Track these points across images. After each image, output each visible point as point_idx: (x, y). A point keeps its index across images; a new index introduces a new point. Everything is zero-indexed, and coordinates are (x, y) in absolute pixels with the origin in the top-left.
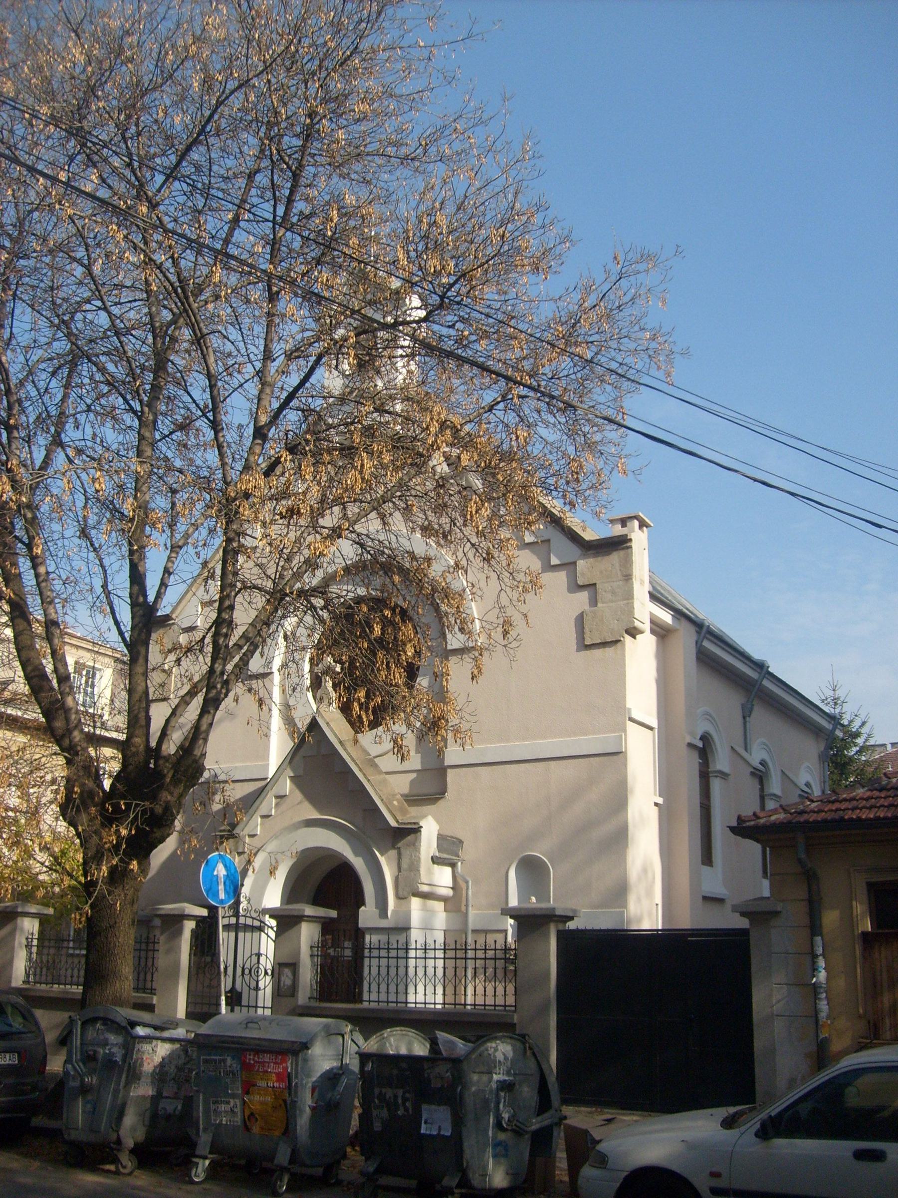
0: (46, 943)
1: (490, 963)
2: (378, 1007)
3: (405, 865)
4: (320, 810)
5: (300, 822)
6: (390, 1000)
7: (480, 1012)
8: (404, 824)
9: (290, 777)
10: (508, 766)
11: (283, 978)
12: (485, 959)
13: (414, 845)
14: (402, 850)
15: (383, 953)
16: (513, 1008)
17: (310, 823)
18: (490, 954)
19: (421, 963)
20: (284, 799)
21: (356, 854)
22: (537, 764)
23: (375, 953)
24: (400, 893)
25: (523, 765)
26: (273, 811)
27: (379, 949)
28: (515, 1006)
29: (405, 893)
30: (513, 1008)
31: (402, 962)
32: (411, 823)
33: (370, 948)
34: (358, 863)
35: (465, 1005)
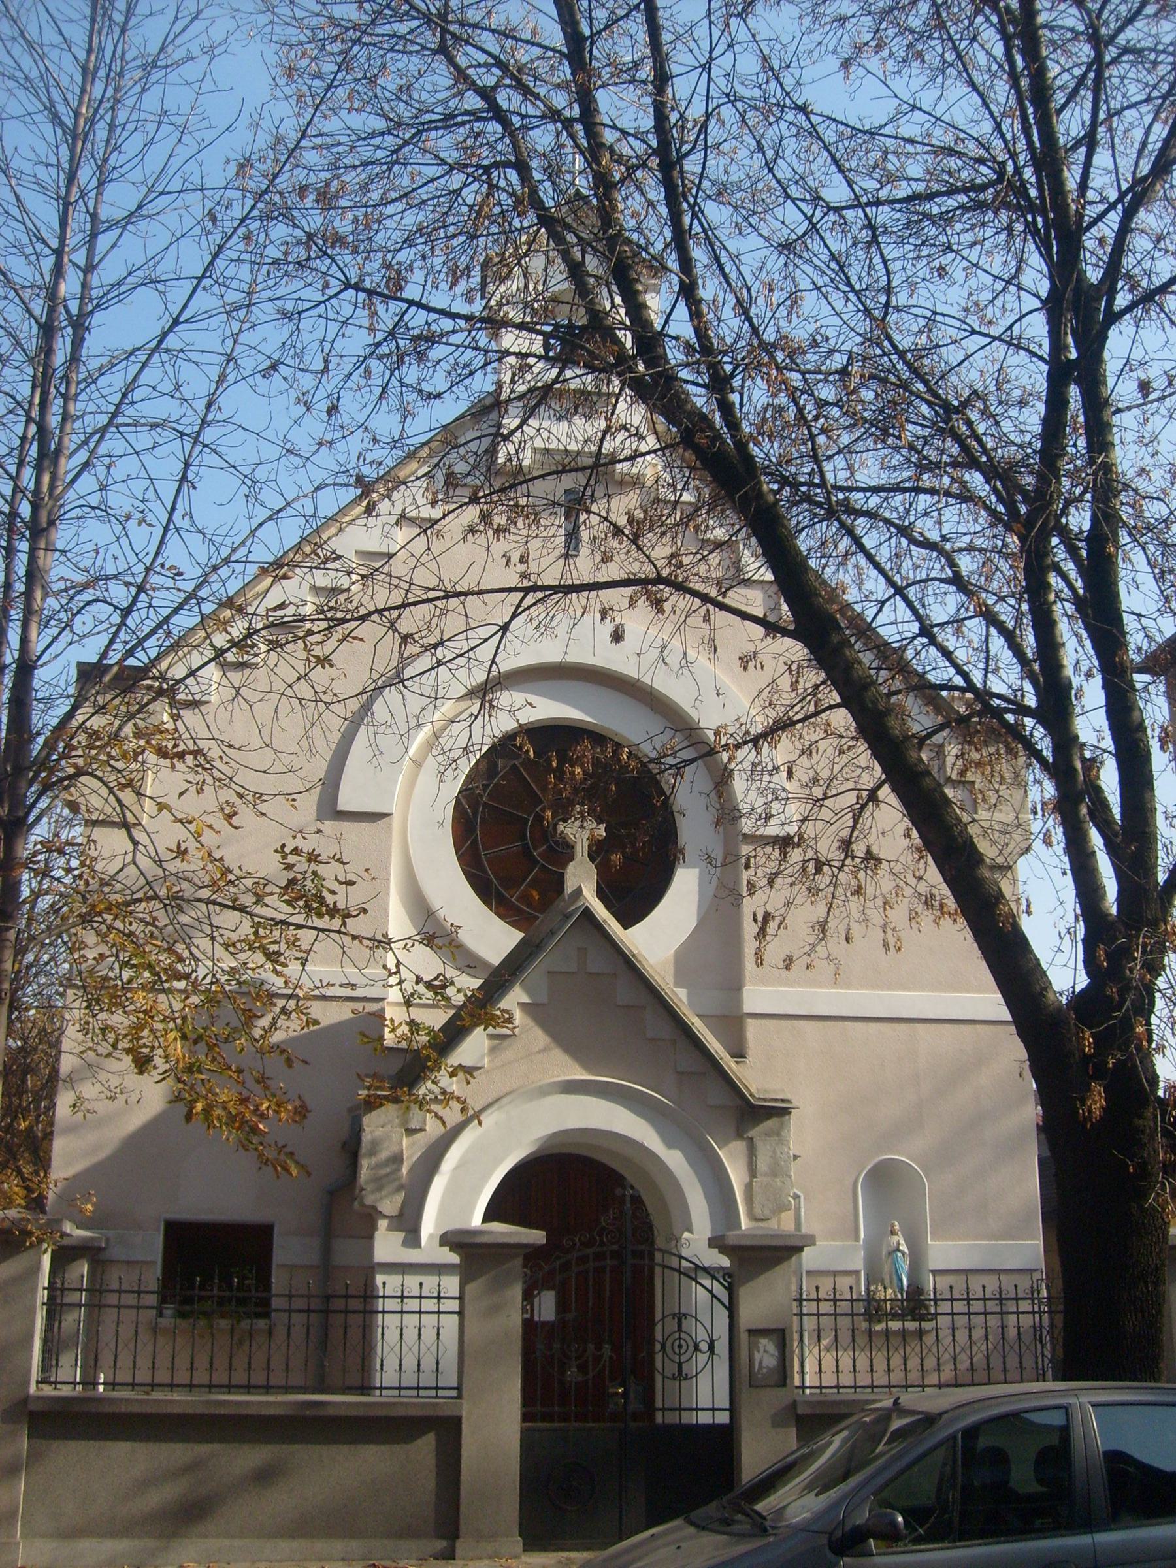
0: (355, 1304)
1: (844, 1322)
2: (838, 1398)
3: (762, 1164)
4: (587, 1066)
5: (550, 1084)
6: (842, 1382)
7: (829, 1398)
8: (765, 1100)
9: (522, 1005)
10: (848, 1024)
11: (757, 1356)
12: (836, 1315)
13: (778, 1134)
14: (758, 1143)
15: (960, 1307)
16: (454, 1393)
17: (571, 1087)
18: (844, 1307)
19: (961, 1321)
20: (507, 1042)
21: (670, 1145)
22: (896, 1026)
23: (945, 1307)
24: (758, 1211)
25: (873, 1026)
26: (486, 1060)
27: (1017, 1299)
28: (459, 1388)
29: (767, 1212)
30: (454, 1393)
31: (355, 1320)
32: (776, 1100)
33: (935, 1300)
34: (675, 1160)
35: (803, 1387)
